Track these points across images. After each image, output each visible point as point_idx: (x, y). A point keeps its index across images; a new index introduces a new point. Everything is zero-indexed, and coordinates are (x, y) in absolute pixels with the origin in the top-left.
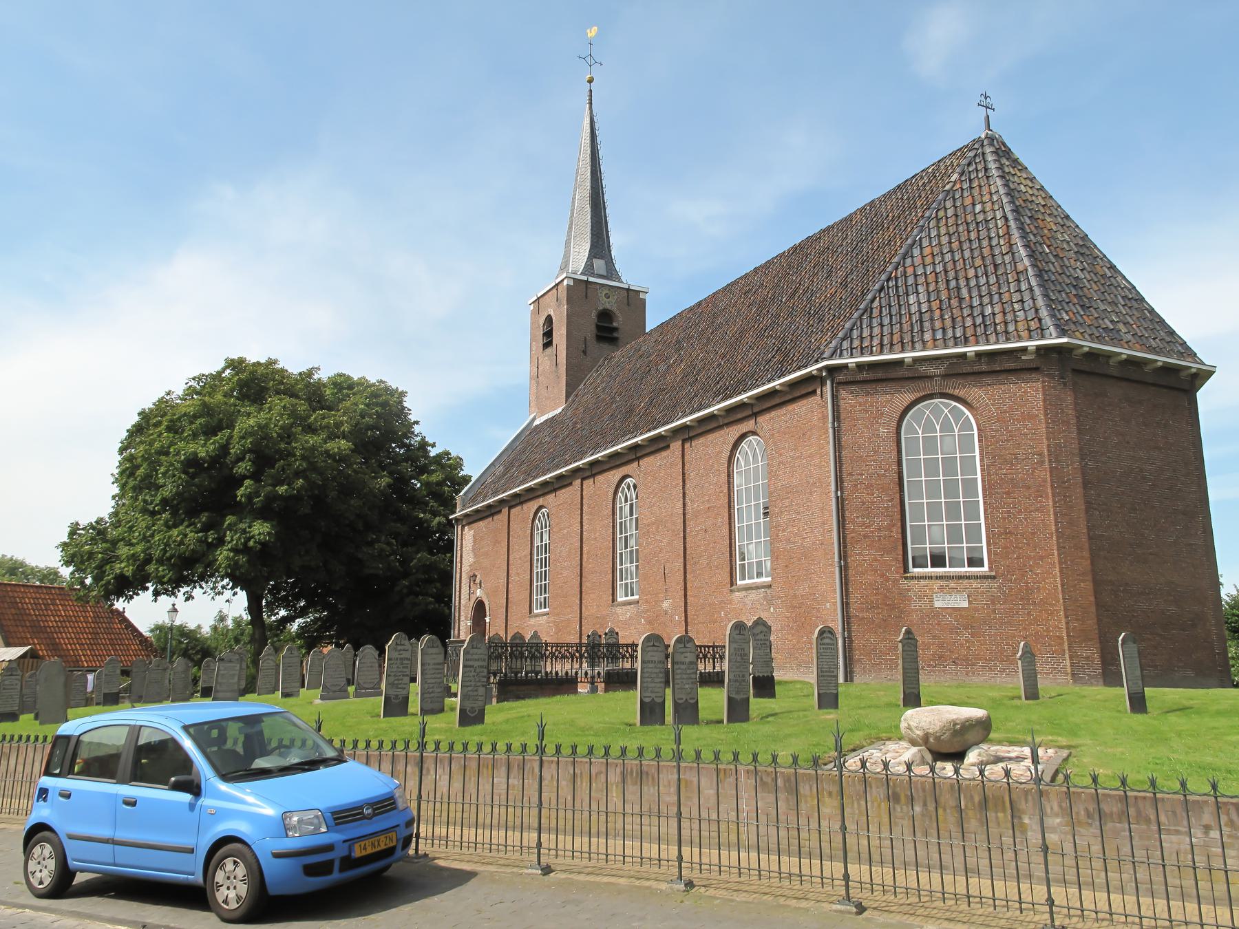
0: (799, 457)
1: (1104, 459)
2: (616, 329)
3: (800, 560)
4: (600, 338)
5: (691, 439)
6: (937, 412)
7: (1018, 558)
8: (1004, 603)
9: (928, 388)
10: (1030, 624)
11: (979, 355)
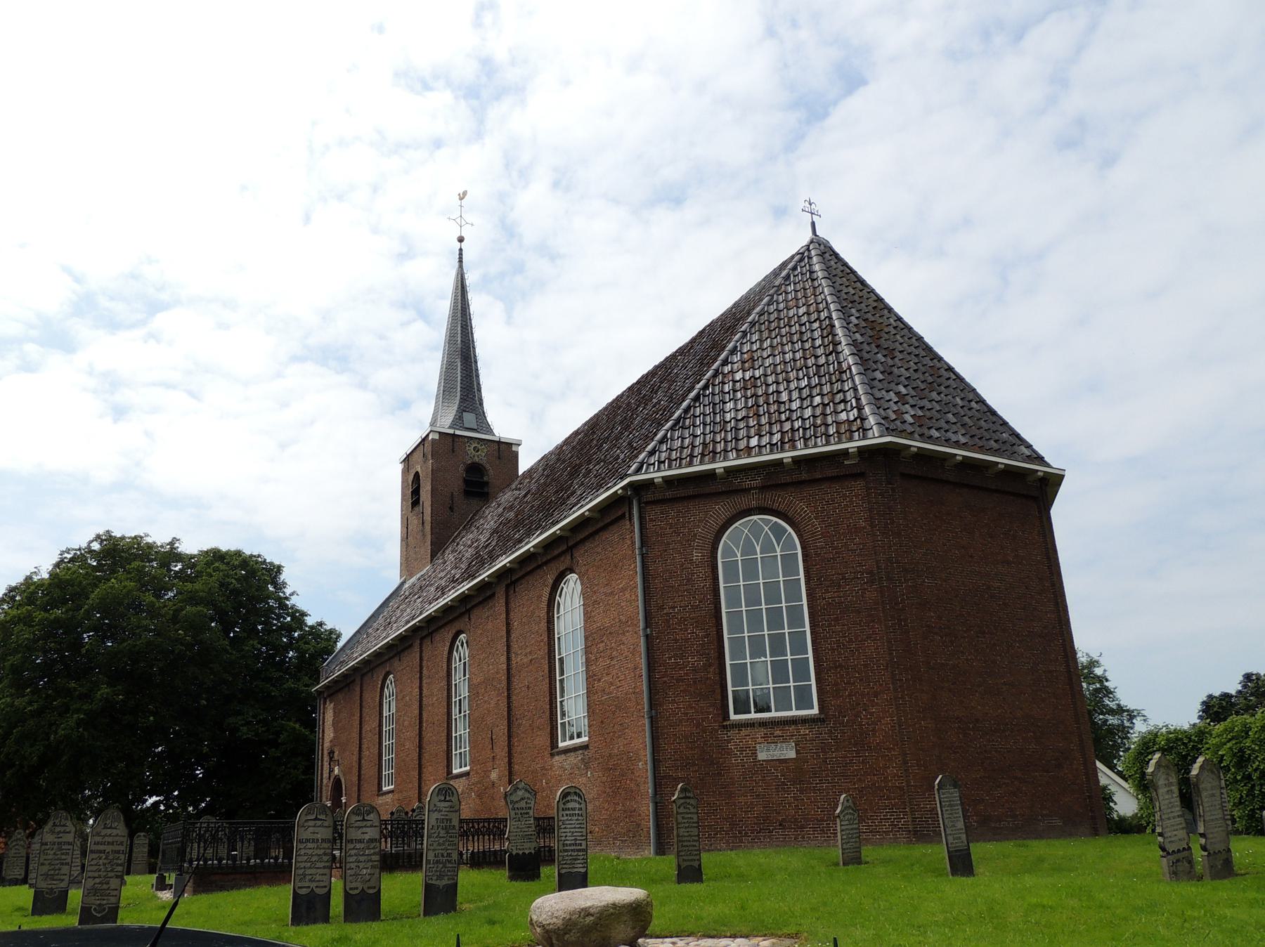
2: (487, 483)
4: (468, 494)
5: (514, 583)
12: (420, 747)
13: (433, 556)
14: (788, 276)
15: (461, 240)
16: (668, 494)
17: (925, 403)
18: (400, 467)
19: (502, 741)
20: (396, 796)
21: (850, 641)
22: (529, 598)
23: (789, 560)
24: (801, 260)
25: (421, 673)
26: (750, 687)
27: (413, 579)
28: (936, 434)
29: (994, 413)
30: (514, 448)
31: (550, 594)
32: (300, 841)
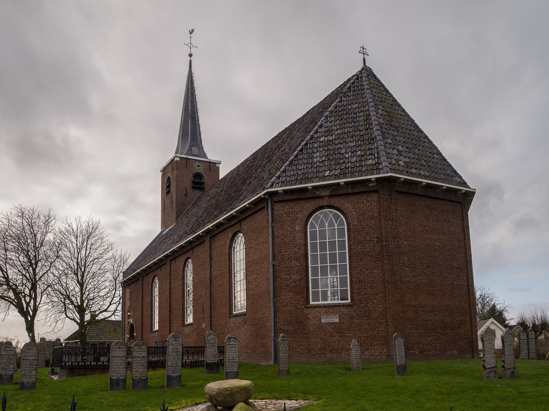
0: (258, 244)
2: (203, 183)
3: (258, 299)
6: (326, 216)
7: (365, 294)
8: (357, 319)
10: (370, 330)
11: (347, 183)
12: (170, 311)
13: (177, 218)
14: (350, 87)
15: (191, 55)
16: (285, 198)
17: (411, 155)
18: (161, 173)
19: (207, 311)
20: (159, 333)
21: (367, 269)
22: (222, 240)
23: (341, 232)
24: (357, 79)
25: (170, 277)
27: (167, 230)
29: (445, 160)
31: (230, 242)
32: (113, 357)
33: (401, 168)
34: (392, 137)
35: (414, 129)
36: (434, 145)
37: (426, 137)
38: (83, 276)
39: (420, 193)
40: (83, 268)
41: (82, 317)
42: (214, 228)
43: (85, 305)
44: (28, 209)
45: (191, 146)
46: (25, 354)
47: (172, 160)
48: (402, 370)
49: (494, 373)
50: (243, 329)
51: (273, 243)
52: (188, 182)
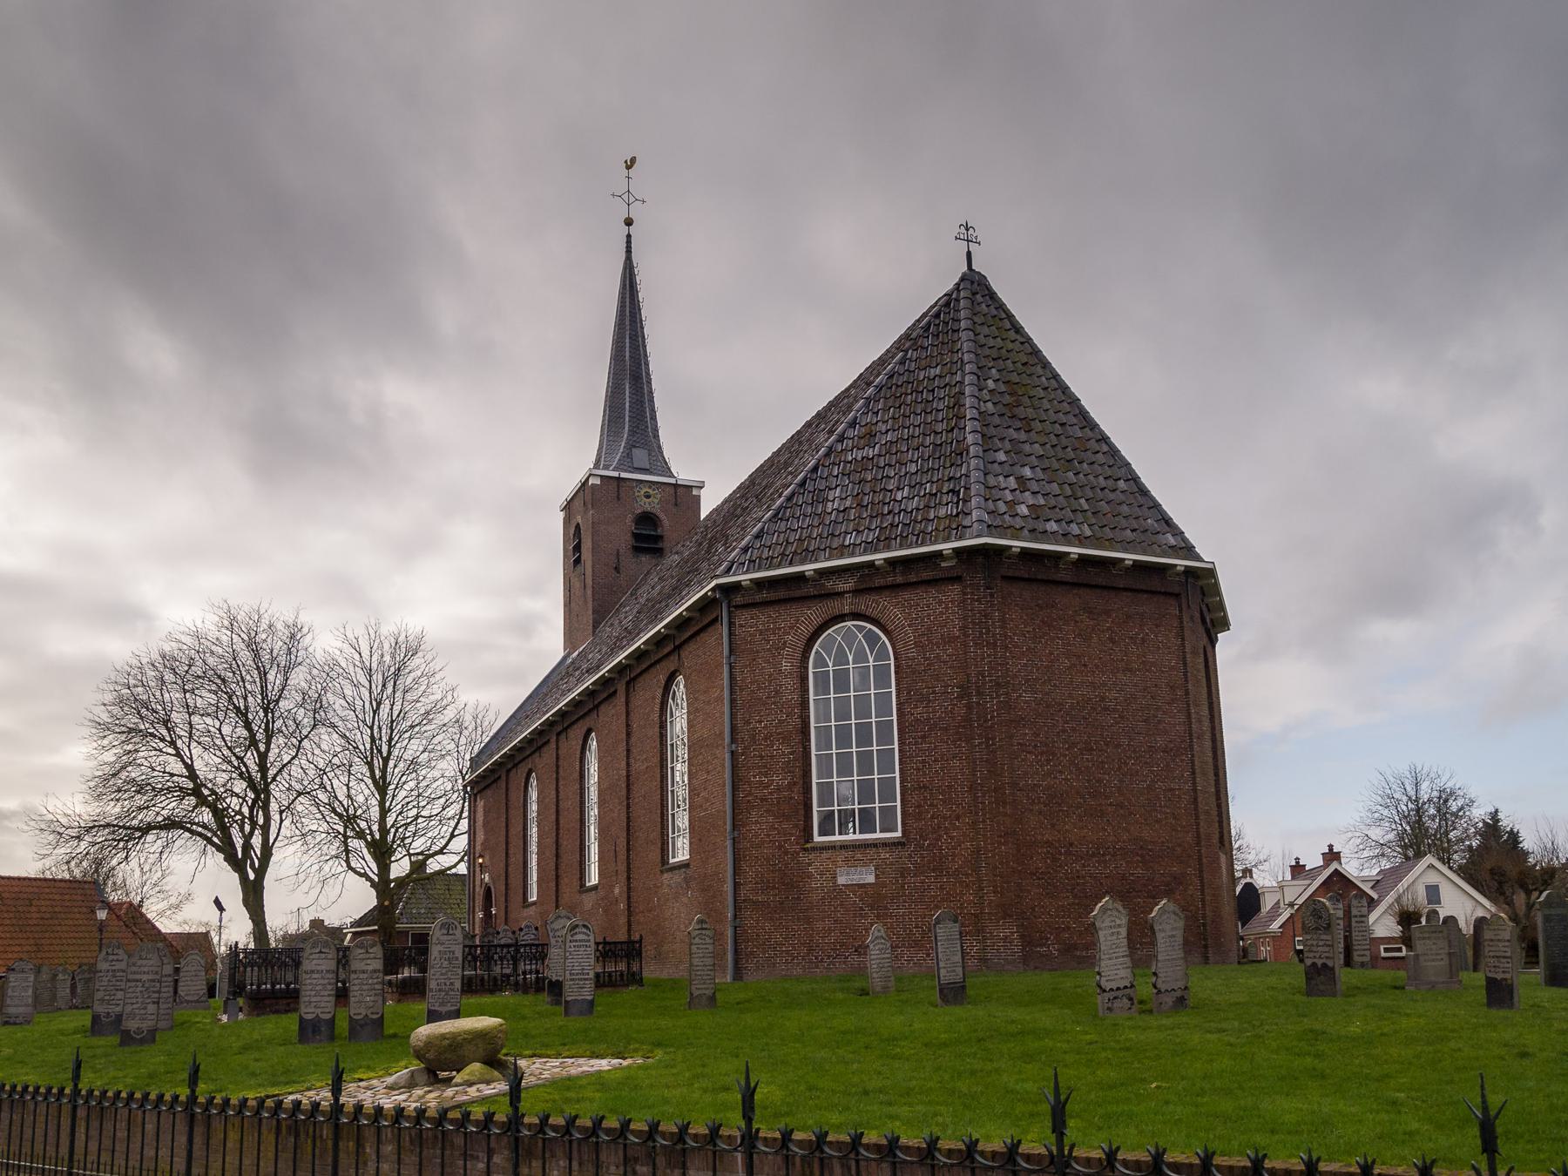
1: (1047, 688)
9: (835, 607)
10: (943, 900)
16: (758, 598)
17: (1055, 488)
18: (562, 515)
23: (882, 673)
26: (856, 806)
28: (1052, 526)
30: (695, 492)
33: (1018, 522)
34: (1008, 446)
35: (1075, 421)
36: (1122, 458)
37: (1104, 439)
38: (384, 771)
39: (1068, 579)
40: (385, 749)
41: (384, 868)
42: (632, 662)
43: (390, 838)
44: (246, 608)
45: (631, 446)
46: (134, 969)
47: (584, 484)
48: (953, 994)
49: (1125, 1000)
50: (685, 900)
51: (733, 701)
52: (621, 534)
